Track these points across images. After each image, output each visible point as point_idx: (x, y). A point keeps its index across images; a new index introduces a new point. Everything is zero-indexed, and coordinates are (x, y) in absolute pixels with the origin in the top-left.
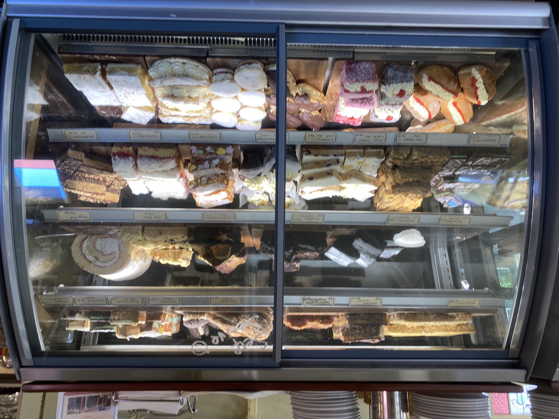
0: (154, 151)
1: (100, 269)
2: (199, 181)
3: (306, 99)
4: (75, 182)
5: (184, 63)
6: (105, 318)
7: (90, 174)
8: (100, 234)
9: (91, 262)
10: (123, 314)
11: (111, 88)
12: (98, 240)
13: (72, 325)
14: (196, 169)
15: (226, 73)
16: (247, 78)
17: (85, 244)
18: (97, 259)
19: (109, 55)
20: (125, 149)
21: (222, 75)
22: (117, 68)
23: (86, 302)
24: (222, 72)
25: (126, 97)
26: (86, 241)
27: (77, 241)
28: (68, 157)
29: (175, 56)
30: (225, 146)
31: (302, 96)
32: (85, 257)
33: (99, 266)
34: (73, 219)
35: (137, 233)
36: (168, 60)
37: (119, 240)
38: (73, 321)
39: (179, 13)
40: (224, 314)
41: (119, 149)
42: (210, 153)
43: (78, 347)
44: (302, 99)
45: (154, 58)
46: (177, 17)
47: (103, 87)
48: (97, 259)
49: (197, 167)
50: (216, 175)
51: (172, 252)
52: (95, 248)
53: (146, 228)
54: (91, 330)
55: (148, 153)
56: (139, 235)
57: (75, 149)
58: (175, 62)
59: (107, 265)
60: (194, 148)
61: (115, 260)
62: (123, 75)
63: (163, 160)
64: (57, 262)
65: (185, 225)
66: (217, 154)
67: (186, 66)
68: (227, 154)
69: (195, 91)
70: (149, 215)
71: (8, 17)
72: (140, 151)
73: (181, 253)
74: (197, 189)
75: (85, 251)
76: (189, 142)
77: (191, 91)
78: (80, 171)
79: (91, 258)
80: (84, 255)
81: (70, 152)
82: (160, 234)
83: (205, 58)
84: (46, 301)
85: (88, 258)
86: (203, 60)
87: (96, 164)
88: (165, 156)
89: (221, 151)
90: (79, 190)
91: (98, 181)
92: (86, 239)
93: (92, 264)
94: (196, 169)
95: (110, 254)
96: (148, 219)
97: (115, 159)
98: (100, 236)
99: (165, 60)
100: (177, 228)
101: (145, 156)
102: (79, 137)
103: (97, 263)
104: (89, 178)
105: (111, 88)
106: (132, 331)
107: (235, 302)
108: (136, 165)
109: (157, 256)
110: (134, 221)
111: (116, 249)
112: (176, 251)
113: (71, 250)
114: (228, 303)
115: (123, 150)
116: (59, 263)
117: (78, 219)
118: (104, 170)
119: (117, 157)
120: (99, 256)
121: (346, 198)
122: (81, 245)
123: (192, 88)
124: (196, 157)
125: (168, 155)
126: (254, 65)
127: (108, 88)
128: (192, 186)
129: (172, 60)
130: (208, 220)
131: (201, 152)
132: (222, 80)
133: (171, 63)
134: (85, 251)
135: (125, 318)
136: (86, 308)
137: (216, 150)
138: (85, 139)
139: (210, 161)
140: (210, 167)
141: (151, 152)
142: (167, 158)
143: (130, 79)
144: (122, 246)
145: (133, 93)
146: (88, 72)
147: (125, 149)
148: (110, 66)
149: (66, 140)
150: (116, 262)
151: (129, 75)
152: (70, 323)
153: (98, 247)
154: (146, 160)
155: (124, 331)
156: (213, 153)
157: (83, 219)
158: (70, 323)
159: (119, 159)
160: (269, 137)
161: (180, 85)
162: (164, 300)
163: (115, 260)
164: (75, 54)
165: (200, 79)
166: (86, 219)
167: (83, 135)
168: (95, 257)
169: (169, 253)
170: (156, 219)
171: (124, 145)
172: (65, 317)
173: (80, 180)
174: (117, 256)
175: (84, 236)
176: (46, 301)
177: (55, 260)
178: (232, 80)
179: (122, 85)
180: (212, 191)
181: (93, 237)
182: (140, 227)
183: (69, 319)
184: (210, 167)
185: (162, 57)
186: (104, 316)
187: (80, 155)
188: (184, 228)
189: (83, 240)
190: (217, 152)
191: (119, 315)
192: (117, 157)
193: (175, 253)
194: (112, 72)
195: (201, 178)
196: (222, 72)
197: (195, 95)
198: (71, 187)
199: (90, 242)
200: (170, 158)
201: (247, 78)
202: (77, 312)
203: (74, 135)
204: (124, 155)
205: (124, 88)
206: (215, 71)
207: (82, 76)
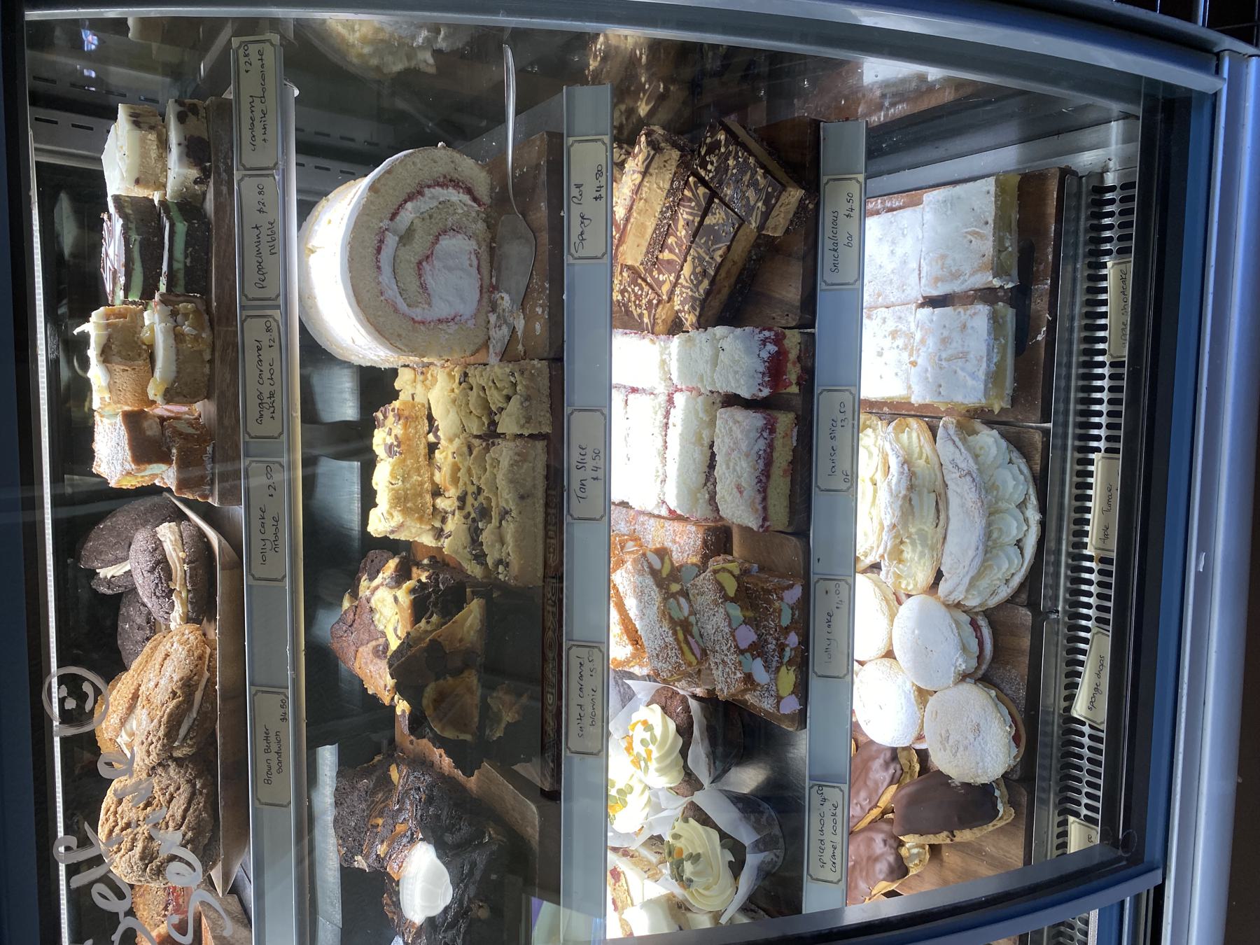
0: (784, 465)
1: (372, 250)
2: (675, 587)
3: (662, 553)
4: (669, 176)
5: (1019, 544)
6: (181, 275)
7: (697, 231)
8: (492, 251)
9: (393, 216)
10: (200, 352)
11: (933, 302)
12: (473, 245)
13: (143, 141)
14: (726, 598)
15: (980, 657)
16: (977, 729)
17: (455, 196)
18: (406, 237)
19: (1051, 326)
20: (793, 373)
21: (973, 644)
22: (1005, 337)
23: (252, 217)
24: (981, 644)
25: (894, 334)
26: (466, 198)
27: (468, 167)
28: (784, 187)
29: (1043, 524)
30: (802, 690)
31: (899, 858)
32: (410, 198)
33: (379, 250)
34: (575, 192)
35: (528, 420)
36: (1033, 500)
37: (475, 316)
38: (164, 144)
39: (1204, 579)
40: (206, 717)
41: (793, 355)
42: (781, 648)
43: (36, 100)
44: (891, 859)
45: (1038, 458)
46: (1197, 573)
47: (937, 280)
48: (406, 237)
49: (733, 600)
50: (704, 652)
51: (421, 484)
52: (445, 232)
53: (540, 445)
54: (117, 199)
55: (778, 444)
56: (522, 427)
57: (801, 205)
58: (1026, 520)
59: (386, 276)
60: (795, 594)
61: (402, 306)
62: (989, 360)
63: (759, 497)
64: (361, 55)
65: (554, 574)
66: (778, 669)
67: (1013, 551)
68: (779, 699)
69: (922, 555)
70: (590, 464)
71: (1218, 56)
72: (785, 420)
73: (421, 519)
74: (649, 581)
75: (433, 198)
76: (813, 578)
77: (924, 544)
78: (710, 202)
79: (409, 214)
80: (420, 193)
81: (794, 195)
82: (522, 497)
83: (1033, 605)
84: (254, 57)
85: (409, 205)
86: (1024, 597)
87: (735, 263)
88: (771, 502)
89: (788, 678)
90: (638, 189)
91: (660, 242)
92: (475, 199)
93: (385, 223)
94: (726, 598)
95: (423, 287)
96: (575, 456)
97: (764, 342)
98: (484, 251)
99: (1032, 491)
100: (540, 547)
101: (772, 440)
102: (835, 222)
103: (391, 240)
104: (674, 217)
105: (933, 302)
106: (125, 378)
107: (268, 781)
108: (731, 400)
109: (405, 426)
110: (567, 410)
111: (441, 309)
112: (428, 498)
113: (939, 772)
114: (262, 757)
115: (789, 365)
116: (355, 60)
117: (576, 211)
118: (712, 283)
119: (772, 348)
120: (419, 245)
121: (375, 487)
122: (455, 183)
123: (932, 549)
124: (770, 602)
125: (771, 510)
126: (1015, 751)
127: (935, 293)
128: (657, 564)
129: (1034, 516)
130: (574, 663)
131: (786, 620)
132: (964, 649)
133: (1022, 506)
134: (433, 198)
135: (182, 359)
136: (222, 207)
137: (790, 663)
138: (829, 244)
139: (757, 649)
140: (742, 652)
141: (782, 457)
142: (765, 509)
143: (973, 375)
144: (453, 327)
145: (914, 364)
146: (1000, 248)
147: (793, 373)
148: (1009, 314)
149: (824, 179)
150: (396, 310)
151: (987, 374)
152: (152, 137)
153: (446, 243)
154: (761, 444)
155: (127, 348)
156: (781, 657)
157: (576, 229)
158: (152, 137)
159: (765, 355)
160: (828, 828)
161: (948, 518)
162: (269, 522)
163: (402, 306)
164: (1059, 220)
165: (972, 584)
166: (574, 238)
167: (842, 239)
168: (410, 231)
169: (418, 470)
170: (575, 485)
171: (803, 369)
172: (181, 118)
173: (672, 192)
174: (417, 313)
175: (483, 190)
176: (254, 57)
177: (366, 50)
178: (964, 677)
179: (945, 342)
180: (638, 625)
181: (481, 226)
182: (547, 429)
183: (174, 138)
184: (742, 652)
185: (1041, 482)
186: (188, 271)
187: (778, 225)
188: (540, 574)
189: (469, 191)
190: (784, 669)
191: (196, 338)
192: (772, 348)
193: (420, 495)
194: (995, 319)
195: (685, 594)
196: (981, 644)
197: (908, 553)
198: (654, 165)
199: (467, 215)
200: (765, 519)
201: (977, 729)
202: (206, 173)
203: (843, 212)
204: (775, 369)
205: (931, 342)
206: (982, 622)
207: (988, 231)
